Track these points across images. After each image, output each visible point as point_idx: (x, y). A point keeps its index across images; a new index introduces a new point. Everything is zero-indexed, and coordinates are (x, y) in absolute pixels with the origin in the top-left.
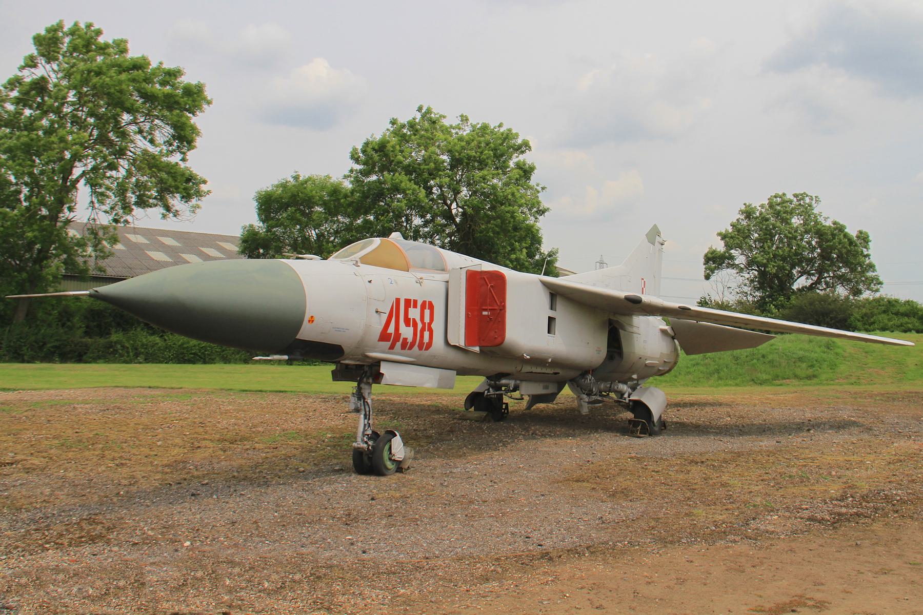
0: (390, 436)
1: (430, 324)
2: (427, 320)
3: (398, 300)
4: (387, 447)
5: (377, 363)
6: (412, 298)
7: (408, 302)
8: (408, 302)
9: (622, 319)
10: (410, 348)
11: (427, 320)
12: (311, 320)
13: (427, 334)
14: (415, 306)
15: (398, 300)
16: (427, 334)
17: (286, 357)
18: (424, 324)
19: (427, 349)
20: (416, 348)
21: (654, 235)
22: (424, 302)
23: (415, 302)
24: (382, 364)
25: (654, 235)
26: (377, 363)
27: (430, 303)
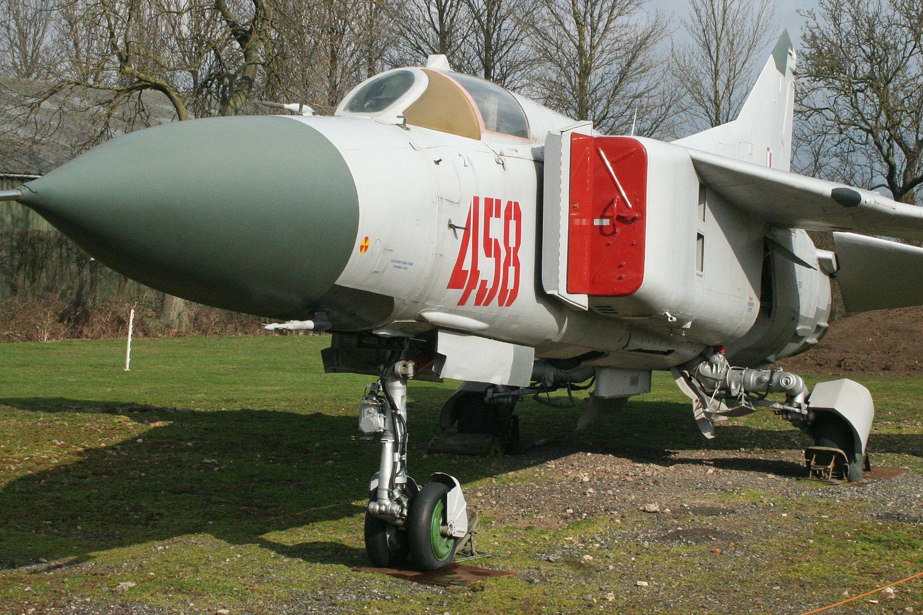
0: (441, 487)
1: (516, 249)
2: (512, 244)
3: (476, 200)
4: (438, 508)
5: (431, 332)
6: (495, 197)
7: (489, 201)
8: (489, 201)
9: (779, 234)
10: (487, 304)
11: (512, 244)
12: (364, 248)
13: (512, 269)
14: (498, 215)
15: (476, 200)
16: (512, 269)
17: (310, 324)
18: (508, 249)
19: (509, 304)
20: (496, 300)
21: (798, 11)
22: (510, 203)
23: (498, 202)
24: (442, 337)
25: (798, 11)
26: (431, 332)
27: (516, 204)
